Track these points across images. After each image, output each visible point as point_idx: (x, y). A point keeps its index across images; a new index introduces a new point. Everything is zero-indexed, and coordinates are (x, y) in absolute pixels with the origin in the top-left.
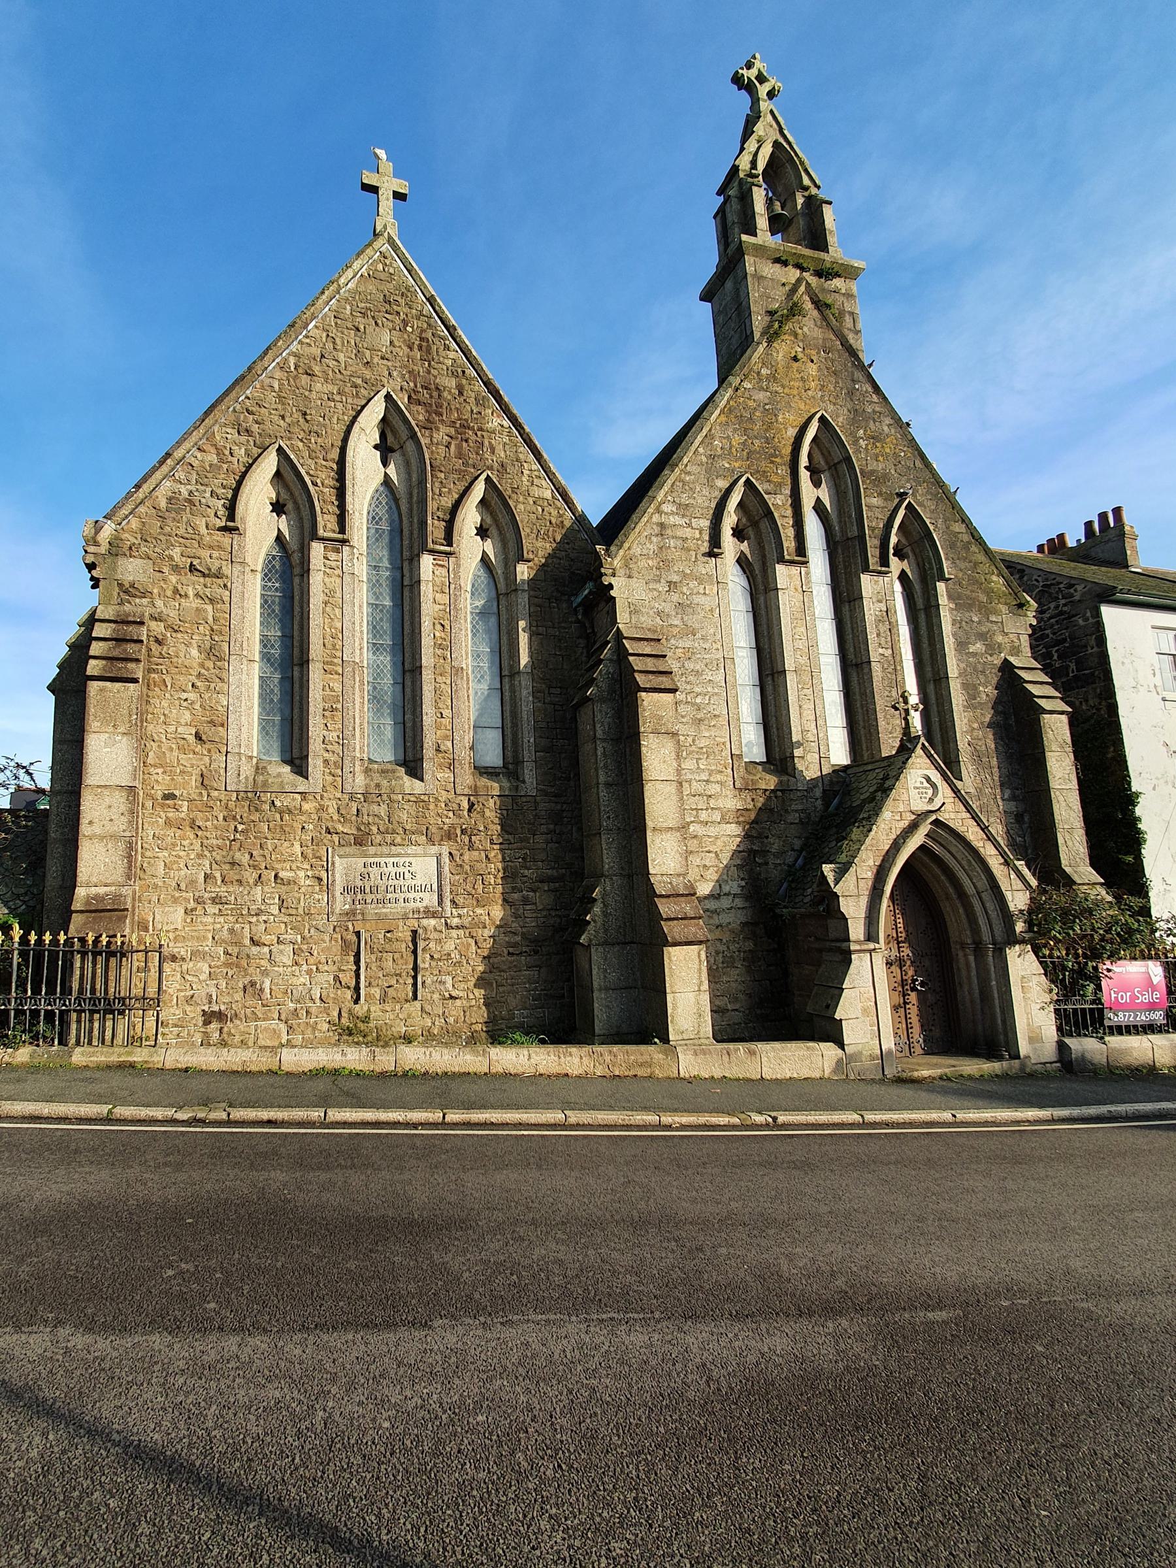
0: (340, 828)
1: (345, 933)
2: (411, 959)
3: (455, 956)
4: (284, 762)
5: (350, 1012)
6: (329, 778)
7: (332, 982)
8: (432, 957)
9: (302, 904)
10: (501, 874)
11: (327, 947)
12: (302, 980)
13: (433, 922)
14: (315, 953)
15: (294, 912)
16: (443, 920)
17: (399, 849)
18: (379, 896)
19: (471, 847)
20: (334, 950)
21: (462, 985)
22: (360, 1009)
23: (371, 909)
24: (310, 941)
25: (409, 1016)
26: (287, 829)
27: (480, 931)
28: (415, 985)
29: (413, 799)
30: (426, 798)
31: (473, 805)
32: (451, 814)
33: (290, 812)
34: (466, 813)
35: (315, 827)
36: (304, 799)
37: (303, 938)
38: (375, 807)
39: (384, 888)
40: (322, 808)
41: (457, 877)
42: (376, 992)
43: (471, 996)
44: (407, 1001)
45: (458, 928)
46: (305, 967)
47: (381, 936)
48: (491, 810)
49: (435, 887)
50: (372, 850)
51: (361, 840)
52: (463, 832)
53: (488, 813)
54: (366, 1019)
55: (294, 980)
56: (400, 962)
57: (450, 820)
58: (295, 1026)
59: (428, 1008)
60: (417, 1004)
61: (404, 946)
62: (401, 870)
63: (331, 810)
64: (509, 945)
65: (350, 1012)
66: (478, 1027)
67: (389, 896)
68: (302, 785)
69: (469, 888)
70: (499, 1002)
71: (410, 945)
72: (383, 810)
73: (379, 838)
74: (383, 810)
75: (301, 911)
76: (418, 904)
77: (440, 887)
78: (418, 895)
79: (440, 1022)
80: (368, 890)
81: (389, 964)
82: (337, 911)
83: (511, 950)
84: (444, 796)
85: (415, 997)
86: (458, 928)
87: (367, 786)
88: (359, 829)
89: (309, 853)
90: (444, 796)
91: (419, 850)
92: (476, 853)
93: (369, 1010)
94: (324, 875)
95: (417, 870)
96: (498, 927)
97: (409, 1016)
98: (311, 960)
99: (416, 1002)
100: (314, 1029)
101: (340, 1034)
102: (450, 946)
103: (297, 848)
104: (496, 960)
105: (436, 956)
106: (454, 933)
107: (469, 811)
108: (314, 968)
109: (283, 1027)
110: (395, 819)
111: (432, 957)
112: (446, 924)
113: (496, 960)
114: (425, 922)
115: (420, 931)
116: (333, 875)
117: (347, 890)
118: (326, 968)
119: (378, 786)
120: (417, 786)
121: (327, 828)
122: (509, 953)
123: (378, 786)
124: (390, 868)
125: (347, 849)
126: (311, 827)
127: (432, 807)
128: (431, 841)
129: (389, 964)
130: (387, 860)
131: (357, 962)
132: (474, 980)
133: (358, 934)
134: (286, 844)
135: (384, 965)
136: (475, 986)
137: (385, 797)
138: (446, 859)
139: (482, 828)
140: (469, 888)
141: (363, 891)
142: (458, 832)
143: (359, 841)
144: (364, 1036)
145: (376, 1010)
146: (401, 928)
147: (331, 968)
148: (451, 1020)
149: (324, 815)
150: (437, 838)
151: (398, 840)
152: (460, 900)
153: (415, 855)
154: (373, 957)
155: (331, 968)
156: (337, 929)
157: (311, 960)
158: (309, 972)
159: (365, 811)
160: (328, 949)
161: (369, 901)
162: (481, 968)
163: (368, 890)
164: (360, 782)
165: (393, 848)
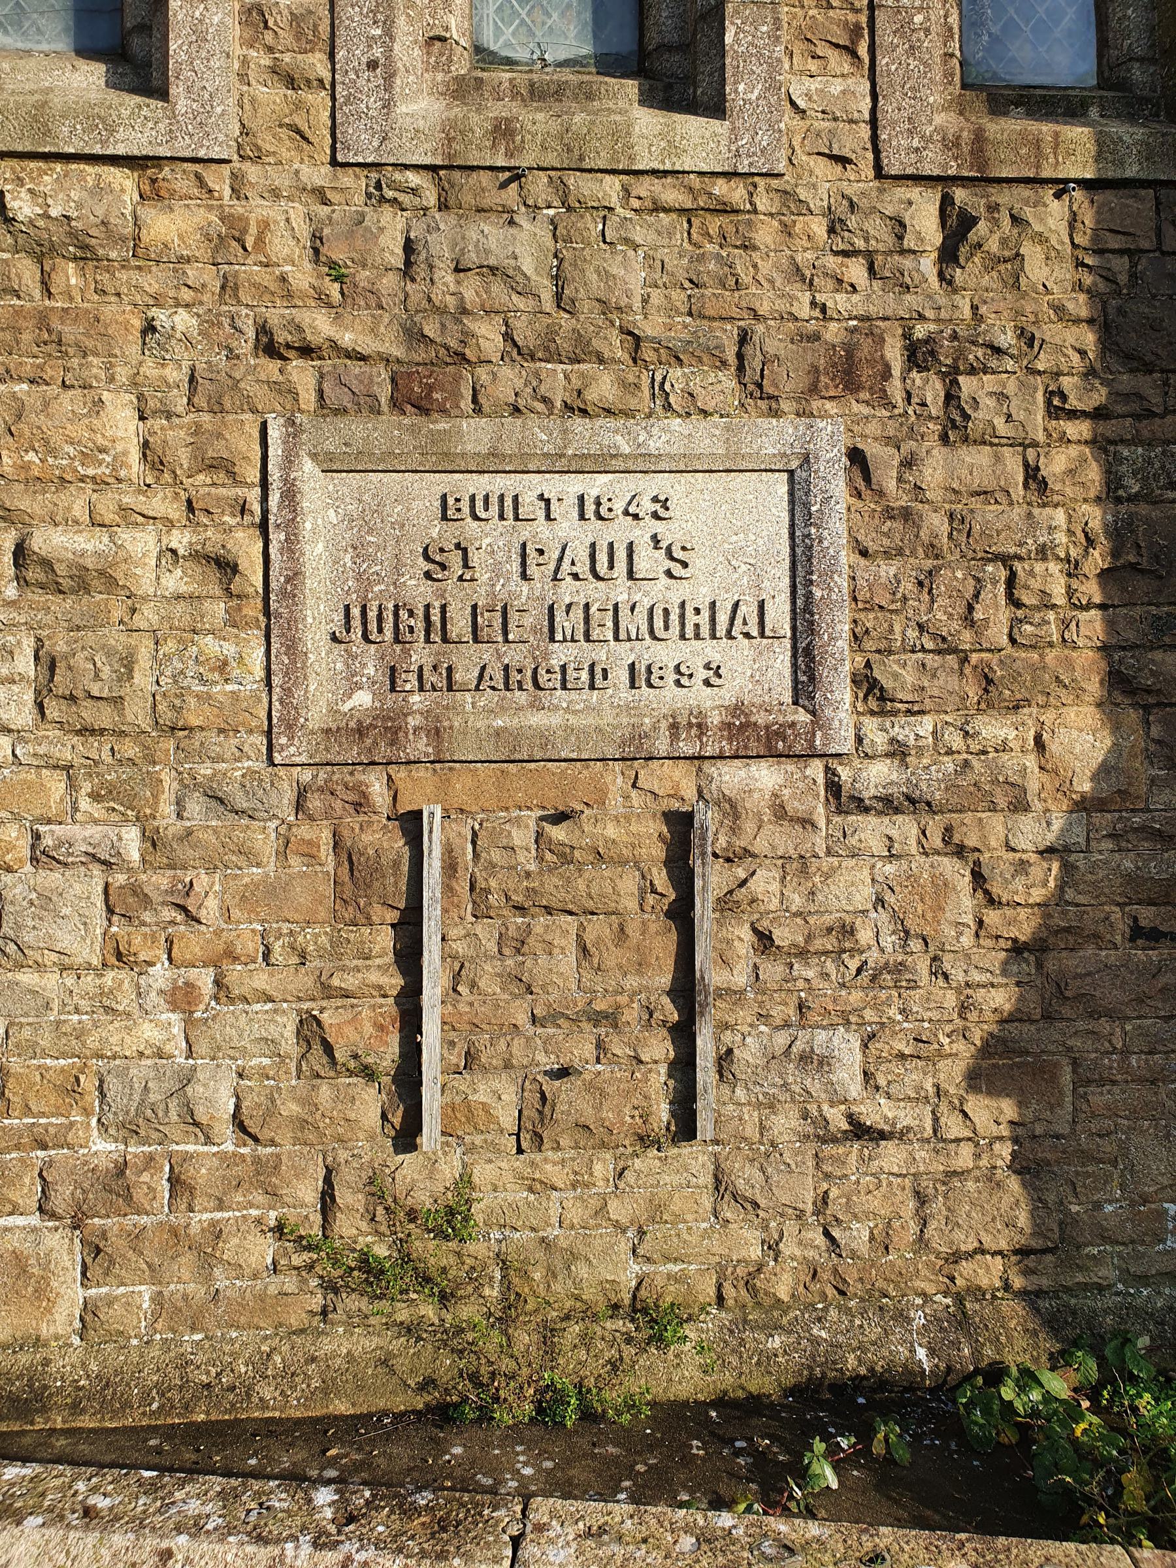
0: (320, 325)
1: (352, 821)
2: (664, 946)
3: (876, 938)
4: (85, 52)
5: (376, 1188)
6: (272, 95)
7: (289, 1044)
8: (764, 940)
9: (143, 679)
10: (1098, 559)
11: (264, 874)
12: (148, 1032)
13: (765, 777)
14: (210, 910)
15: (104, 717)
16: (816, 770)
17: (613, 436)
18: (514, 655)
19: (956, 426)
20: (301, 896)
21: (915, 1077)
22: (424, 1175)
23: (477, 715)
24: (185, 853)
25: (657, 1211)
26: (70, 332)
27: (996, 825)
28: (684, 1065)
29: (672, 195)
30: (736, 193)
31: (968, 222)
32: (856, 271)
33: (86, 255)
34: (928, 265)
35: (209, 323)
36: (153, 194)
37: (152, 841)
38: (490, 238)
39: (534, 617)
40: (232, 237)
41: (887, 570)
42: (500, 1098)
43: (954, 1127)
44: (645, 1141)
45: (888, 805)
46: (160, 975)
47: (522, 837)
48: (1051, 249)
49: (779, 615)
50: (475, 434)
51: (422, 387)
52: (919, 355)
53: (1036, 269)
54: (452, 1220)
55: (113, 1035)
56: (613, 957)
57: (857, 297)
58: (116, 1244)
59: (746, 1177)
60: (695, 1159)
61: (629, 883)
62: (620, 532)
63: (281, 246)
64: (1136, 889)
65: (376, 1188)
66: (988, 1273)
67: (560, 654)
68: (138, 126)
69: (945, 618)
70: (1087, 1157)
71: (661, 879)
72: (526, 247)
73: (508, 381)
74: (526, 247)
75: (137, 713)
76: (698, 696)
77: (804, 614)
78: (696, 654)
79: (802, 1244)
80: (460, 625)
81: (559, 969)
82: (316, 716)
83: (1147, 915)
84: (821, 183)
85: (685, 1126)
86: (888, 805)
87: (452, 132)
88: (414, 336)
89: (176, 440)
90: (821, 183)
91: (705, 437)
92: (977, 458)
93: (465, 1180)
94: (246, 549)
95: (698, 536)
96: (1083, 806)
97: (657, 1211)
98: (192, 943)
99: (686, 1150)
100: (207, 1260)
101: (331, 1287)
102: (850, 889)
103: (121, 424)
104: (1072, 962)
105: (783, 936)
106: (871, 831)
107: (948, 255)
108: (205, 979)
109: (62, 1249)
110: (587, 285)
111: (764, 940)
112: (834, 787)
113: (1072, 962)
114: (730, 777)
115: (708, 817)
116: (291, 546)
117: (358, 622)
118: (261, 980)
119: (503, 131)
120: (697, 141)
121: (263, 329)
122: (1137, 933)
123: (503, 131)
124: (567, 526)
125: (358, 429)
126: (184, 321)
127: (766, 234)
128: (759, 393)
129: (559, 969)
130: (552, 485)
131: (409, 957)
132: (964, 1052)
133: (411, 825)
134: (69, 402)
135: (538, 967)
136: (976, 1080)
137: (539, 186)
138: (834, 483)
139: (1007, 339)
140: (945, 618)
141: (437, 627)
142: (894, 353)
143: (415, 396)
144: (444, 1298)
145: (498, 1179)
146: (615, 802)
147: (290, 980)
148: (857, 1236)
149: (250, 270)
150: (788, 381)
151: (604, 387)
152: (900, 676)
153: (687, 466)
154: (486, 932)
155: (290, 980)
156: (315, 803)
157: (192, 943)
158: (182, 998)
159: (440, 247)
160: (270, 894)
161: (466, 675)
162: (1001, 999)
163: (460, 625)
164: (419, 111)
165: (578, 424)
